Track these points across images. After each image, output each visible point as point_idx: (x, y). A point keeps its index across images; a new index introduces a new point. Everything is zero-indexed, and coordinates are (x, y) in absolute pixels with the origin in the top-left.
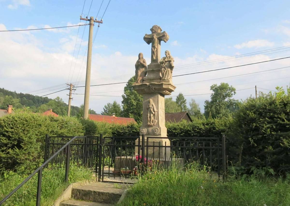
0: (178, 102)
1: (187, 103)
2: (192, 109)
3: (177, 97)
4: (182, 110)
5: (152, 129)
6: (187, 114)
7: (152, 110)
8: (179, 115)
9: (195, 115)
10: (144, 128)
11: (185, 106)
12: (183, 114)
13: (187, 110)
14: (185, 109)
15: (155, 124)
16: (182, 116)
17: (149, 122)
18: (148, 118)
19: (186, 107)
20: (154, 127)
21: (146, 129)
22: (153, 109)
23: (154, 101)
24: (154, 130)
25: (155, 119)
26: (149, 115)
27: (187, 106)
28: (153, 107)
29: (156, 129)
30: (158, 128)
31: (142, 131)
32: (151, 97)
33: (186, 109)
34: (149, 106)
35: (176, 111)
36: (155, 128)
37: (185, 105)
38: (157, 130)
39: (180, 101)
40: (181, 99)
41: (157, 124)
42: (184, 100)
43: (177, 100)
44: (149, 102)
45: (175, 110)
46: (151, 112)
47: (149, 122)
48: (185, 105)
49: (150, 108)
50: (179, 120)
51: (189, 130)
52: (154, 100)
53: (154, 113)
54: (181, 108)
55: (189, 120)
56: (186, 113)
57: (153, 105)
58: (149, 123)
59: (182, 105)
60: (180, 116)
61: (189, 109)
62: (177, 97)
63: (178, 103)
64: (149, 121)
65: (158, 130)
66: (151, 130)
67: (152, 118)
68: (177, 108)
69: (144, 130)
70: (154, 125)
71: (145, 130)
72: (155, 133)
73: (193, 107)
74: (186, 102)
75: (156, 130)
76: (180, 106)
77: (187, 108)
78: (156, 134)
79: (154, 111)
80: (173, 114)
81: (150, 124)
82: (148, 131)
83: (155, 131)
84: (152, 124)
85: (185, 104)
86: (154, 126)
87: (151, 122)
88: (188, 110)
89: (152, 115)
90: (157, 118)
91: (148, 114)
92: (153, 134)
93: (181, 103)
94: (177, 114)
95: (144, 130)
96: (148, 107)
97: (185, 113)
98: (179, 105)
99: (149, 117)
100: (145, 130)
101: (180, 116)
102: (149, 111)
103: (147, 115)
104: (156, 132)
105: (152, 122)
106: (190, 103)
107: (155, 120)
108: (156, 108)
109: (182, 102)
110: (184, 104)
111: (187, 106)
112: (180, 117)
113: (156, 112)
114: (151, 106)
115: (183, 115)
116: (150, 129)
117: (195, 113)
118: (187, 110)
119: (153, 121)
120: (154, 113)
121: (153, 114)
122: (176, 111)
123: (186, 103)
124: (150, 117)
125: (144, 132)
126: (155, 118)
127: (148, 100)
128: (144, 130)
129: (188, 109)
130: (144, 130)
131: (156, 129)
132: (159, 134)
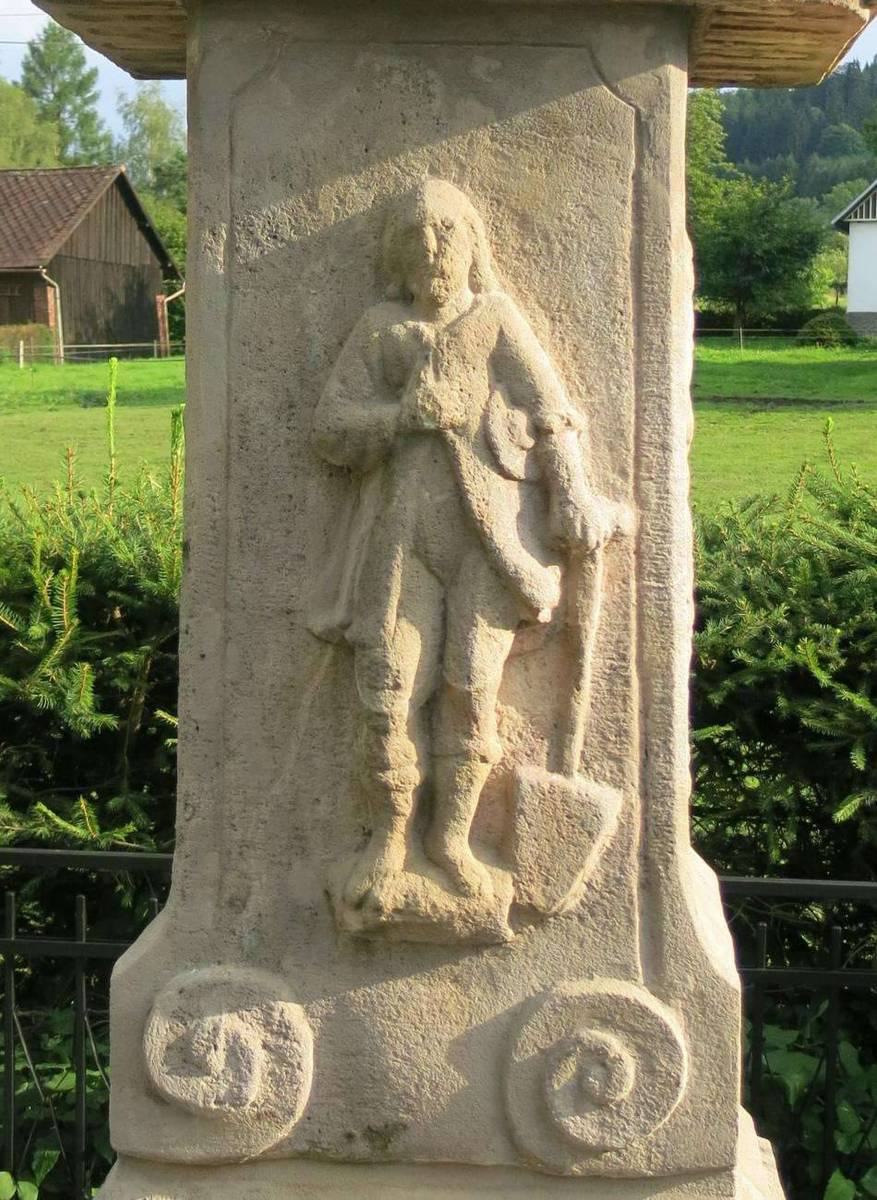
0: (37, 87)
1: (103, 97)
2: (134, 139)
3: (34, 50)
4: (63, 146)
5: (491, 1007)
6: (122, 182)
7: (500, 507)
8: (57, 184)
9: (159, 187)
10: (240, 999)
11: (87, 120)
12: (89, 180)
13: (103, 147)
14: (85, 143)
15: (572, 899)
16: (78, 198)
17: (397, 850)
18: (380, 727)
19: (100, 127)
20: (523, 973)
21: (293, 1013)
22: (544, 488)
23: (523, 228)
24: (550, 1059)
25: (558, 764)
26: (406, 650)
27: (102, 122)
28: (540, 431)
29: (616, 1044)
30: (660, 986)
31: (186, 1058)
32: (440, 128)
33: (95, 143)
34: (396, 374)
35: (26, 154)
36: (577, 988)
37: (88, 108)
38: (630, 1066)
39: (53, 78)
40: (61, 68)
41: (615, 882)
42: (86, 70)
43: (27, 68)
44: (400, 268)
45: (16, 143)
46: (462, 567)
47: (397, 850)
48: (88, 108)
49: (431, 439)
50: (58, 231)
51: (799, 681)
52: (524, 221)
53: (544, 584)
54: (62, 131)
55: (135, 226)
56: (110, 179)
57: (508, 373)
58: (397, 880)
59: (69, 107)
60: (64, 194)
61: (116, 141)
62: (27, 51)
63: (35, 94)
64: (406, 803)
65: (648, 1068)
66: (458, 1052)
67: (497, 735)
68: (30, 127)
69: (260, 1057)
70: (525, 914)
71: (280, 1056)
72: (582, 1127)
73: (145, 129)
74: (94, 89)
75: (600, 1057)
76: (49, 115)
77: (101, 133)
78: (598, 1151)
79: (563, 547)
80: (11, 180)
81: (434, 897)
82: (350, 1058)
83: (568, 1071)
84: (491, 888)
85: (86, 102)
86: (542, 940)
87: (458, 845)
88: (109, 147)
89: (491, 648)
90: (609, 734)
91: (371, 597)
92: (493, 1153)
93: (58, 96)
94: (45, 183)
95: (237, 1055)
96: (387, 413)
97: (103, 175)
98: (43, 108)
99: (400, 706)
100: (280, 1056)
101: (64, 194)
102: (419, 552)
103: (352, 656)
104: (584, 1097)
105: (498, 844)
106: (121, 96)
107: (579, 784)
108: (608, 436)
109: (65, 86)
110: (78, 100)
111: (101, 115)
112: (68, 202)
113: (600, 573)
114: (457, 394)
115: (90, 191)
116: (427, 1024)
117: (157, 171)
118: (103, 147)
119: (505, 793)
120: (544, 584)
121: (516, 609)
122: (26, 154)
123: (94, 98)
124: (444, 708)
125: (256, 1089)
126: (559, 729)
127: (353, 196)
128: (260, 1057)
129: (107, 139)
130: (253, 1037)
131: (616, 1044)
132: (686, 1159)
